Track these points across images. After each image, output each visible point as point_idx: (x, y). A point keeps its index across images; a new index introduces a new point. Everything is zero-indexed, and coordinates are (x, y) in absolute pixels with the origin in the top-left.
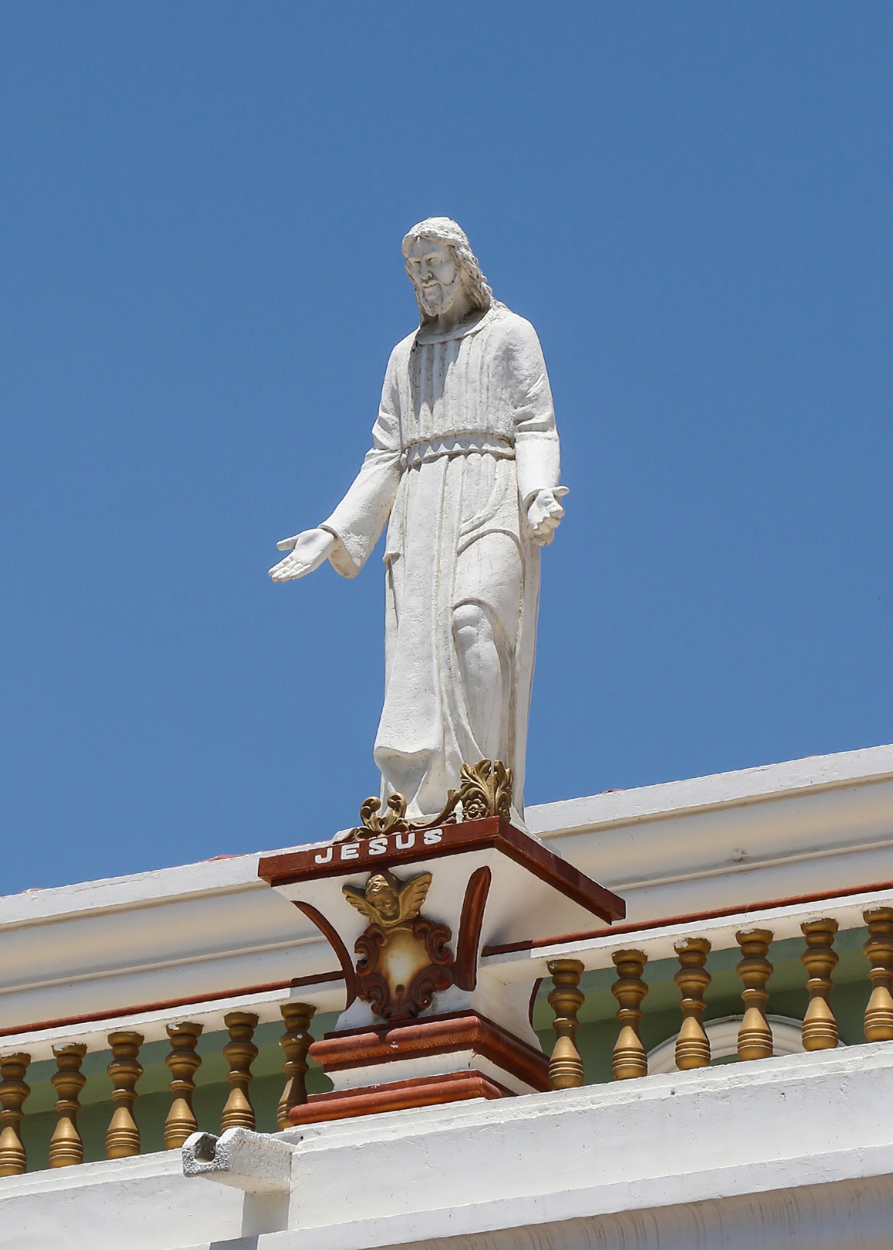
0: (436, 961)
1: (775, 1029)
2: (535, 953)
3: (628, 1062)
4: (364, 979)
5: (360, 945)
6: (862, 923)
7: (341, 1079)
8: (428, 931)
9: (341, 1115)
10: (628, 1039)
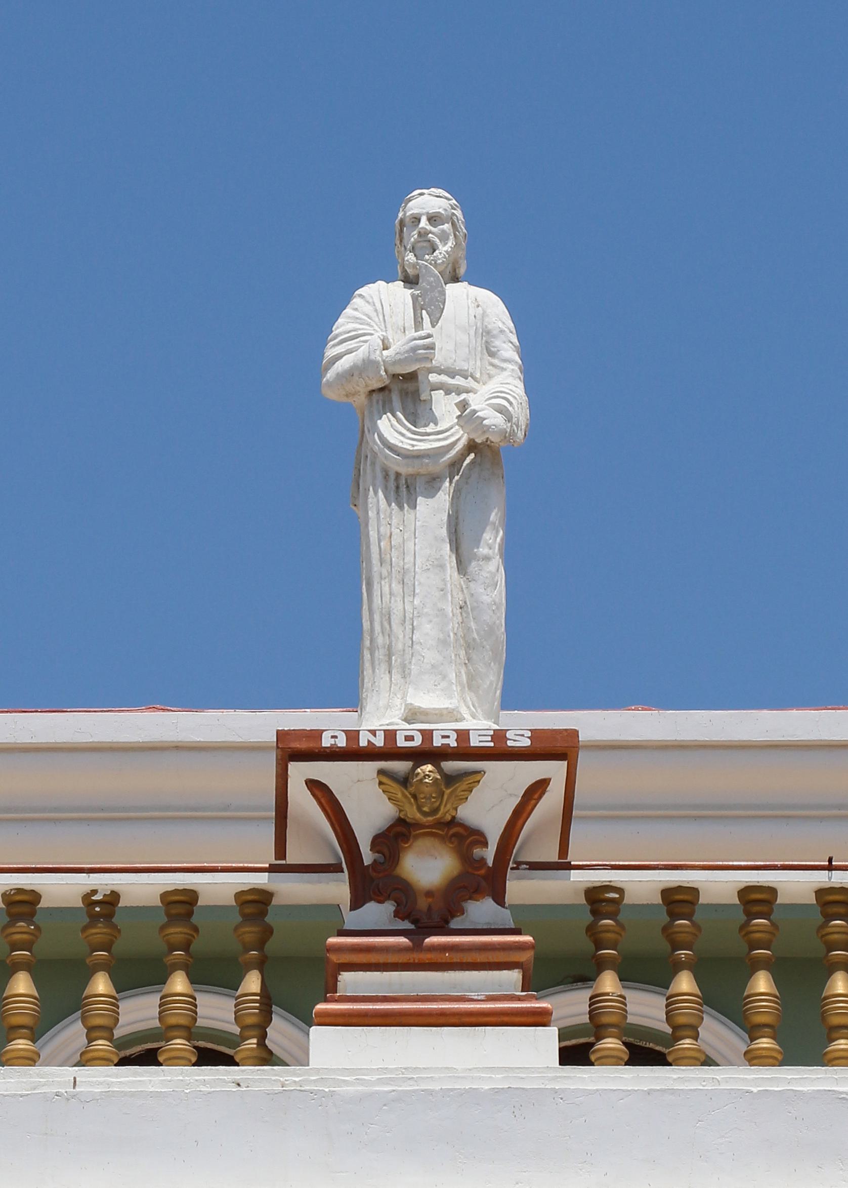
0: (470, 870)
1: (198, 996)
2: (575, 875)
3: (100, 1009)
4: (374, 879)
5: (377, 842)
6: (465, 905)
7: (349, 981)
8: (464, 838)
9: (366, 1021)
10: (101, 985)
